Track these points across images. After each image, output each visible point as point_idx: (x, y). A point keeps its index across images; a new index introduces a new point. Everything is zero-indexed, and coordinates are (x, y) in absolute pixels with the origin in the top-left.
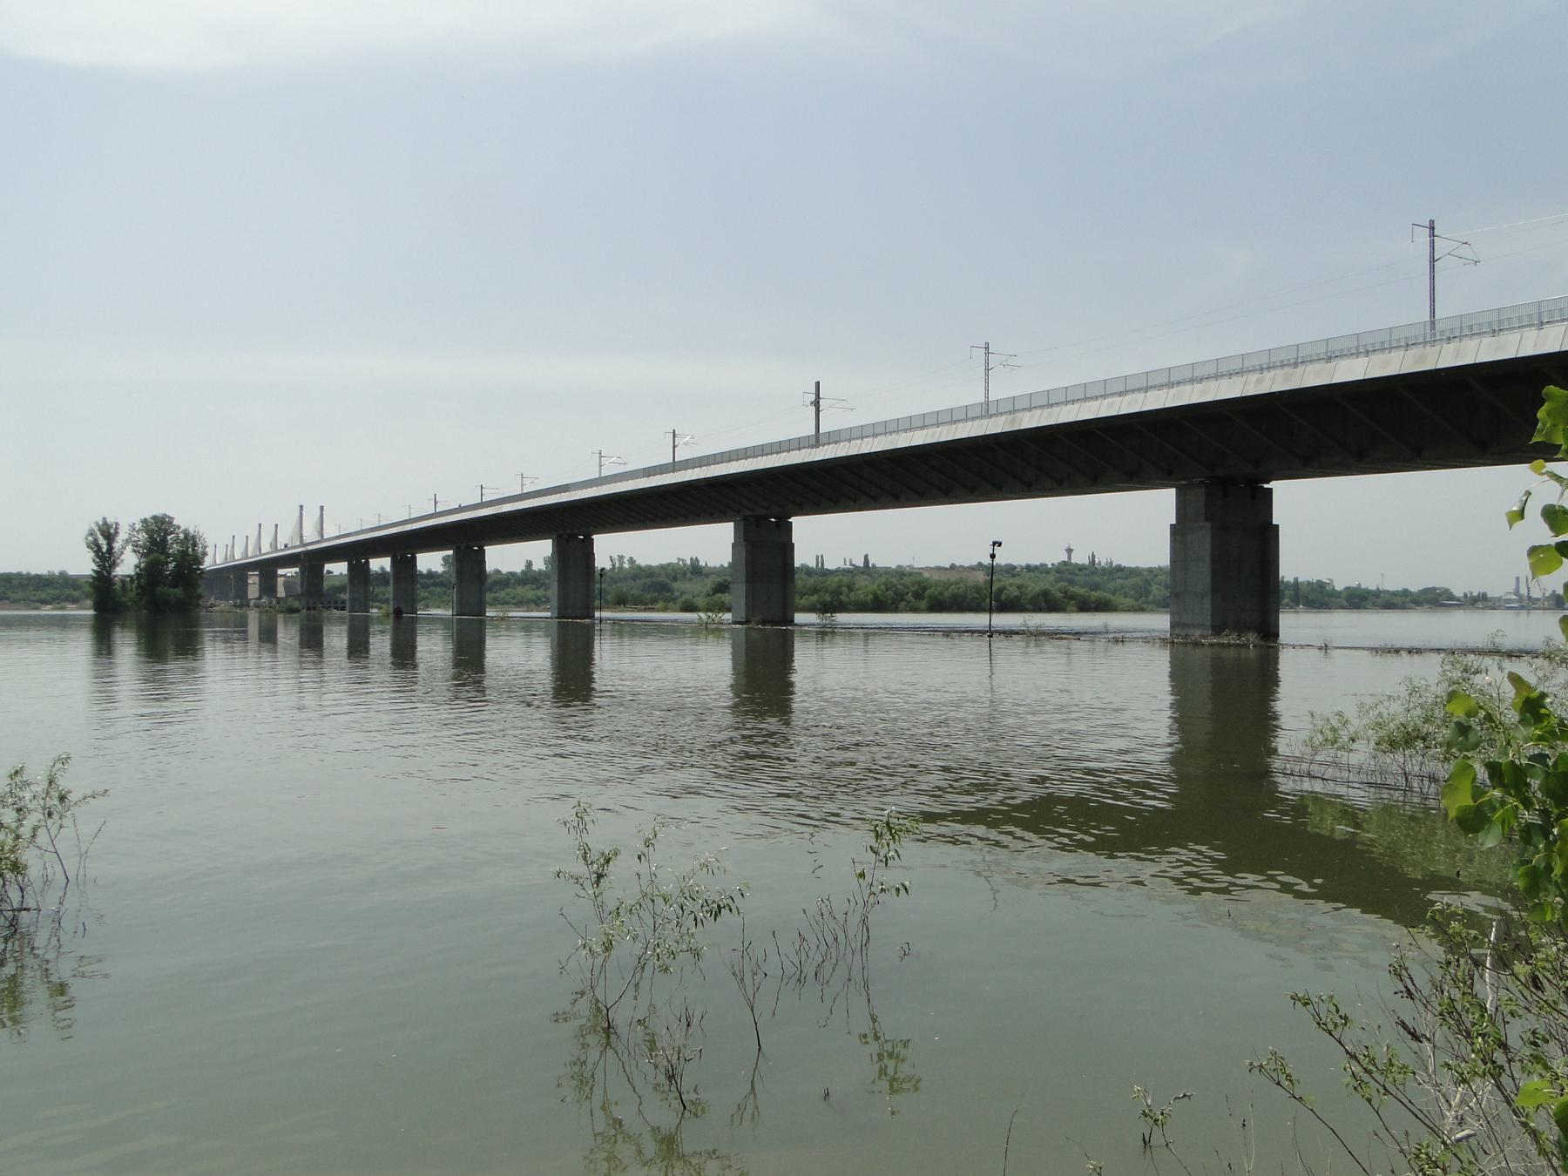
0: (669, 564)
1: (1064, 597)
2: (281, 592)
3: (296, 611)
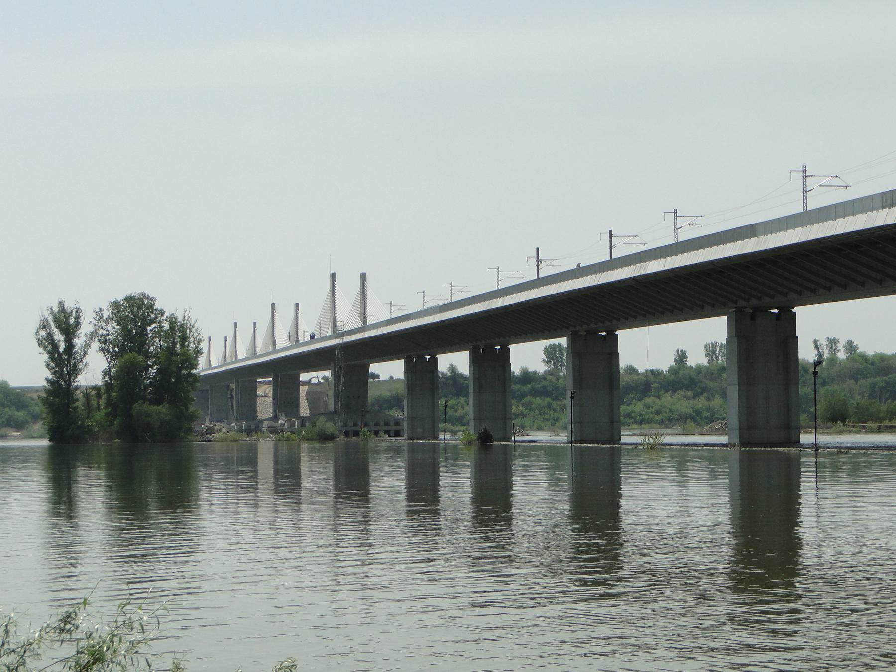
2: (305, 410)
3: (330, 437)
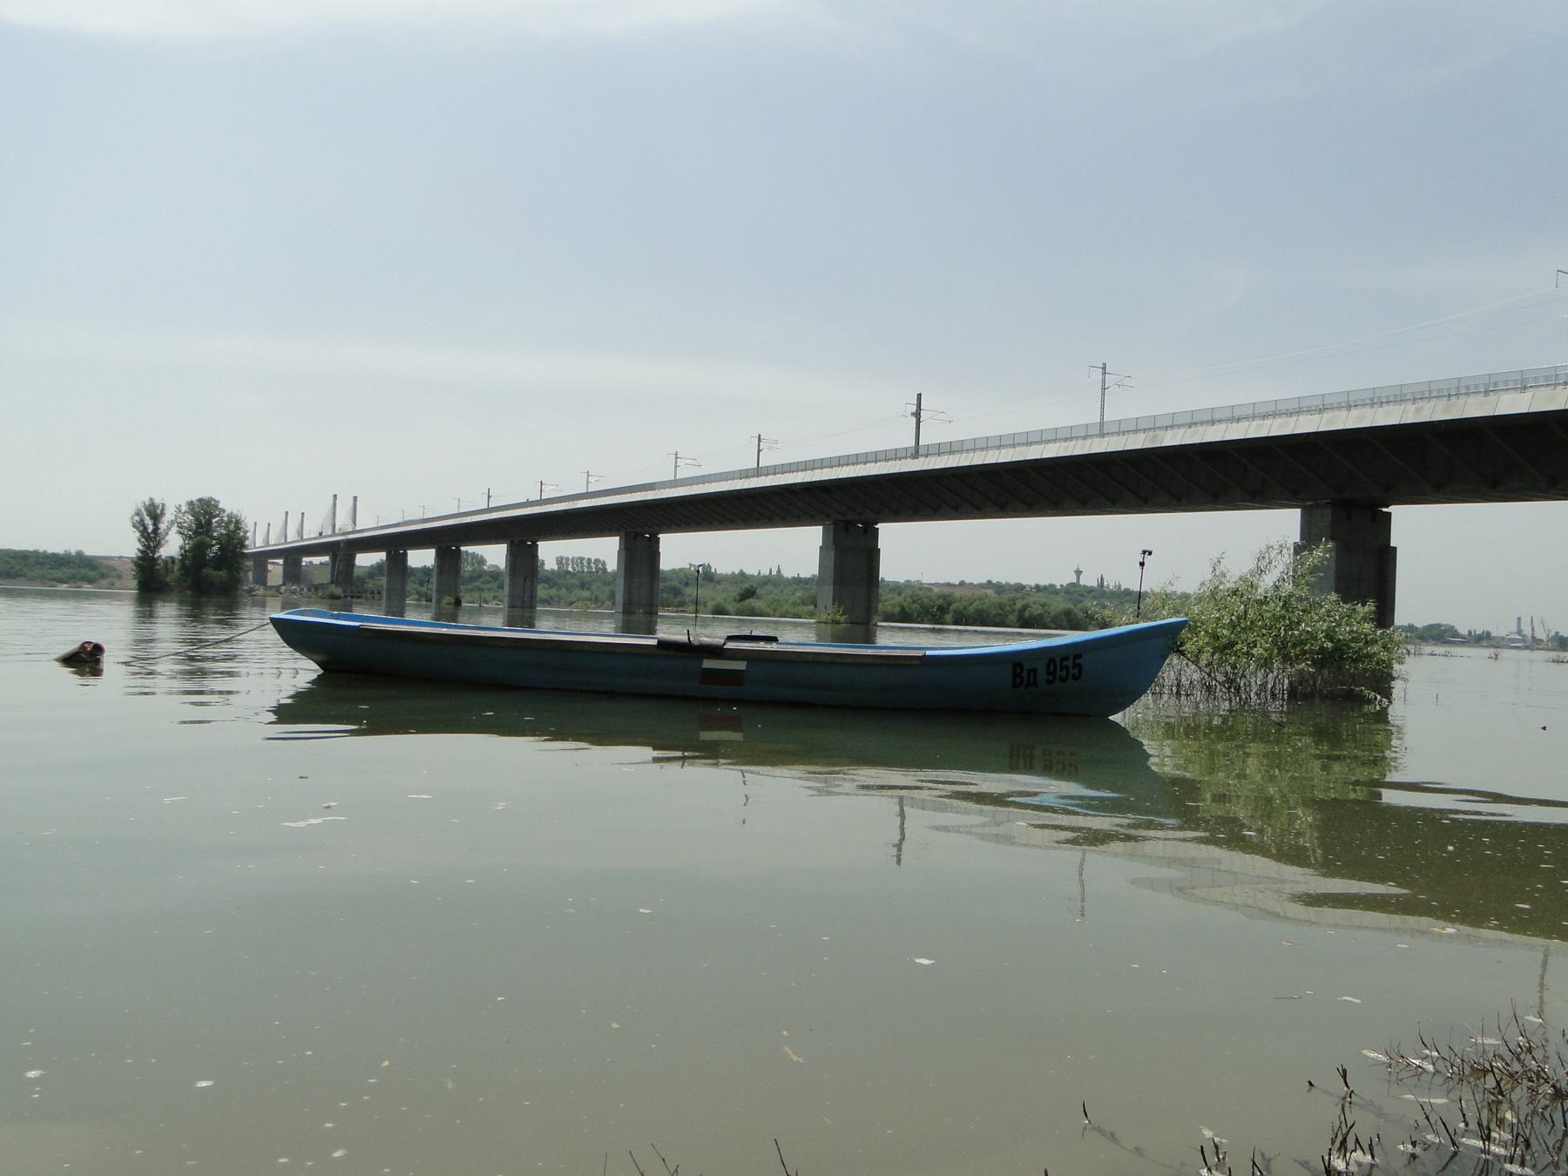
0: (681, 570)
1: (1086, 617)
3: (338, 598)
